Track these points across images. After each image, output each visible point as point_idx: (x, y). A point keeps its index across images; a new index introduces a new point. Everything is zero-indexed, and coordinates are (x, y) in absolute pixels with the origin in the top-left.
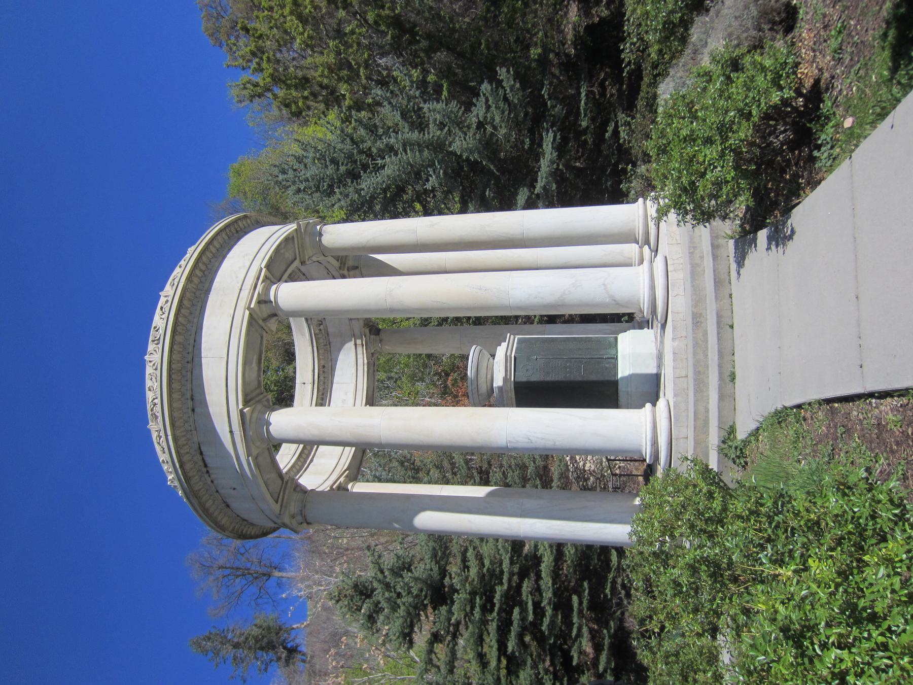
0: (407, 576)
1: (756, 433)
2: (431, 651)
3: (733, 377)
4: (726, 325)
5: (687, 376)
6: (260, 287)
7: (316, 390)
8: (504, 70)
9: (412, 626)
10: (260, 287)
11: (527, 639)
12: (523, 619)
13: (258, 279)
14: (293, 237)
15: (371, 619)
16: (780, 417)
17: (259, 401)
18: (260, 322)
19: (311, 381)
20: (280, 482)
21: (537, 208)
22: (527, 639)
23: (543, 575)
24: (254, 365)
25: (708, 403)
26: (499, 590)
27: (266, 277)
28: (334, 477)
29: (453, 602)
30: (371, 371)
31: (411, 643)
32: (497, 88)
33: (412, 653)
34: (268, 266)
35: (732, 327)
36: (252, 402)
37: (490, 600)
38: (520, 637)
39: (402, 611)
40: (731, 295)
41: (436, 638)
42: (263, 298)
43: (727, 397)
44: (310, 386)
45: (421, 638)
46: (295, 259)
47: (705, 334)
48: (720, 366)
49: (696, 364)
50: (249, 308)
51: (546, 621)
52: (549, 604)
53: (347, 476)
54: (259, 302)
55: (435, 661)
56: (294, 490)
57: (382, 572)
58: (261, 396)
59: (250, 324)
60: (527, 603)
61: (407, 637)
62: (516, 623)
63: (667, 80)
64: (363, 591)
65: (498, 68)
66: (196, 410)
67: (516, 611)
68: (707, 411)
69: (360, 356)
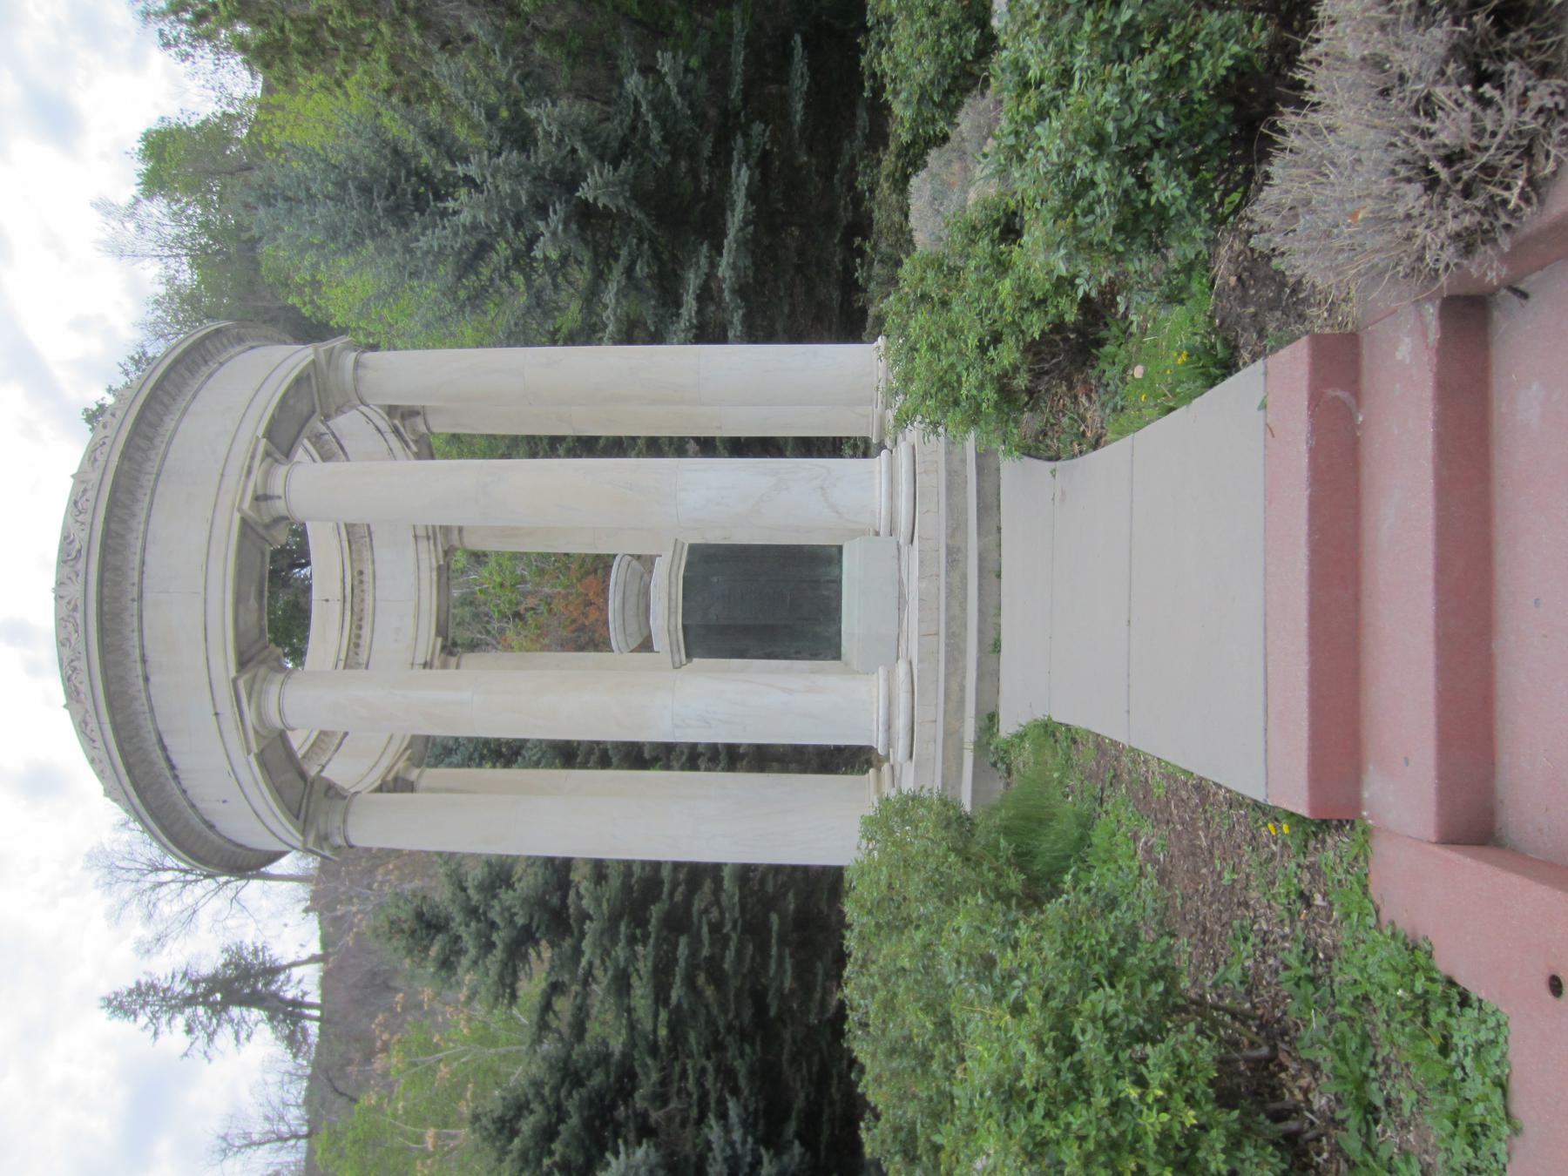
0: (507, 897)
1: (1021, 737)
2: (547, 1006)
3: (997, 647)
4: (991, 572)
5: (937, 634)
6: (257, 474)
7: (348, 613)
8: (669, 55)
9: (515, 974)
10: (257, 474)
11: (701, 979)
12: (694, 953)
13: (253, 457)
14: (309, 376)
15: (447, 964)
16: (1048, 730)
17: (262, 662)
18: (260, 530)
19: (340, 597)
20: (302, 784)
21: (745, 872)
22: (701, 979)
23: (726, 884)
24: (253, 603)
25: (964, 677)
26: (656, 911)
27: (267, 454)
28: (386, 761)
29: (582, 935)
30: (444, 580)
31: (514, 997)
32: (656, 85)
33: (515, 1011)
34: (269, 434)
35: (999, 576)
36: (250, 665)
37: (642, 922)
38: (690, 981)
39: (498, 953)
40: (999, 529)
41: (556, 988)
42: (260, 492)
43: (989, 675)
44: (338, 607)
45: (532, 987)
46: (314, 412)
47: (964, 577)
48: (980, 631)
49: (950, 619)
50: (240, 510)
51: (730, 955)
52: (734, 927)
53: (409, 759)
54: (257, 498)
55: (554, 1024)
56: (326, 794)
57: (464, 889)
58: (266, 652)
59: (243, 535)
60: (700, 928)
61: (507, 988)
62: (682, 963)
63: (923, 174)
64: (429, 924)
65: (659, 54)
66: (152, 679)
67: (683, 941)
68: (962, 689)
69: (424, 556)
